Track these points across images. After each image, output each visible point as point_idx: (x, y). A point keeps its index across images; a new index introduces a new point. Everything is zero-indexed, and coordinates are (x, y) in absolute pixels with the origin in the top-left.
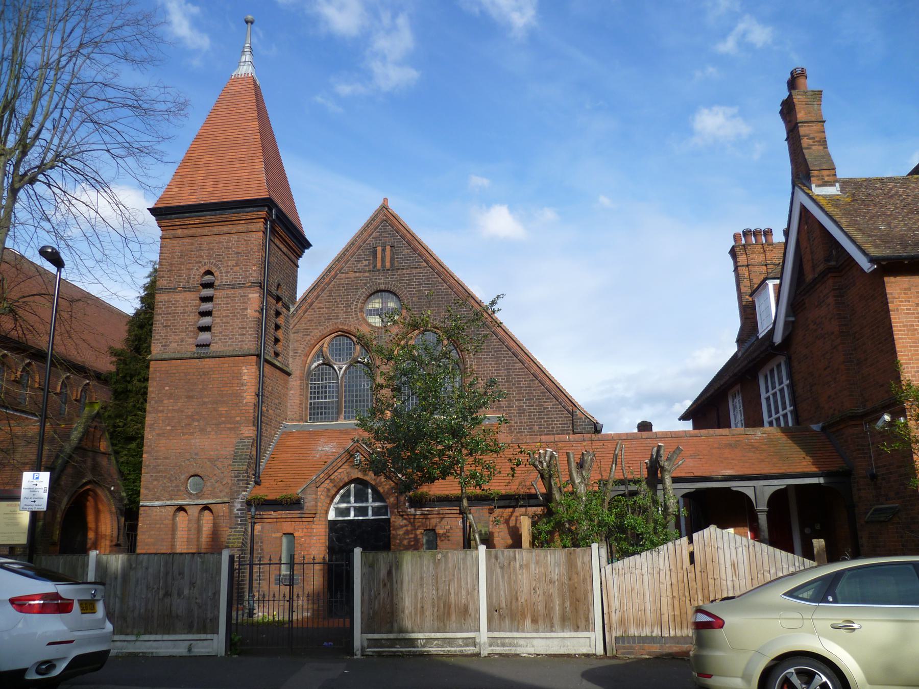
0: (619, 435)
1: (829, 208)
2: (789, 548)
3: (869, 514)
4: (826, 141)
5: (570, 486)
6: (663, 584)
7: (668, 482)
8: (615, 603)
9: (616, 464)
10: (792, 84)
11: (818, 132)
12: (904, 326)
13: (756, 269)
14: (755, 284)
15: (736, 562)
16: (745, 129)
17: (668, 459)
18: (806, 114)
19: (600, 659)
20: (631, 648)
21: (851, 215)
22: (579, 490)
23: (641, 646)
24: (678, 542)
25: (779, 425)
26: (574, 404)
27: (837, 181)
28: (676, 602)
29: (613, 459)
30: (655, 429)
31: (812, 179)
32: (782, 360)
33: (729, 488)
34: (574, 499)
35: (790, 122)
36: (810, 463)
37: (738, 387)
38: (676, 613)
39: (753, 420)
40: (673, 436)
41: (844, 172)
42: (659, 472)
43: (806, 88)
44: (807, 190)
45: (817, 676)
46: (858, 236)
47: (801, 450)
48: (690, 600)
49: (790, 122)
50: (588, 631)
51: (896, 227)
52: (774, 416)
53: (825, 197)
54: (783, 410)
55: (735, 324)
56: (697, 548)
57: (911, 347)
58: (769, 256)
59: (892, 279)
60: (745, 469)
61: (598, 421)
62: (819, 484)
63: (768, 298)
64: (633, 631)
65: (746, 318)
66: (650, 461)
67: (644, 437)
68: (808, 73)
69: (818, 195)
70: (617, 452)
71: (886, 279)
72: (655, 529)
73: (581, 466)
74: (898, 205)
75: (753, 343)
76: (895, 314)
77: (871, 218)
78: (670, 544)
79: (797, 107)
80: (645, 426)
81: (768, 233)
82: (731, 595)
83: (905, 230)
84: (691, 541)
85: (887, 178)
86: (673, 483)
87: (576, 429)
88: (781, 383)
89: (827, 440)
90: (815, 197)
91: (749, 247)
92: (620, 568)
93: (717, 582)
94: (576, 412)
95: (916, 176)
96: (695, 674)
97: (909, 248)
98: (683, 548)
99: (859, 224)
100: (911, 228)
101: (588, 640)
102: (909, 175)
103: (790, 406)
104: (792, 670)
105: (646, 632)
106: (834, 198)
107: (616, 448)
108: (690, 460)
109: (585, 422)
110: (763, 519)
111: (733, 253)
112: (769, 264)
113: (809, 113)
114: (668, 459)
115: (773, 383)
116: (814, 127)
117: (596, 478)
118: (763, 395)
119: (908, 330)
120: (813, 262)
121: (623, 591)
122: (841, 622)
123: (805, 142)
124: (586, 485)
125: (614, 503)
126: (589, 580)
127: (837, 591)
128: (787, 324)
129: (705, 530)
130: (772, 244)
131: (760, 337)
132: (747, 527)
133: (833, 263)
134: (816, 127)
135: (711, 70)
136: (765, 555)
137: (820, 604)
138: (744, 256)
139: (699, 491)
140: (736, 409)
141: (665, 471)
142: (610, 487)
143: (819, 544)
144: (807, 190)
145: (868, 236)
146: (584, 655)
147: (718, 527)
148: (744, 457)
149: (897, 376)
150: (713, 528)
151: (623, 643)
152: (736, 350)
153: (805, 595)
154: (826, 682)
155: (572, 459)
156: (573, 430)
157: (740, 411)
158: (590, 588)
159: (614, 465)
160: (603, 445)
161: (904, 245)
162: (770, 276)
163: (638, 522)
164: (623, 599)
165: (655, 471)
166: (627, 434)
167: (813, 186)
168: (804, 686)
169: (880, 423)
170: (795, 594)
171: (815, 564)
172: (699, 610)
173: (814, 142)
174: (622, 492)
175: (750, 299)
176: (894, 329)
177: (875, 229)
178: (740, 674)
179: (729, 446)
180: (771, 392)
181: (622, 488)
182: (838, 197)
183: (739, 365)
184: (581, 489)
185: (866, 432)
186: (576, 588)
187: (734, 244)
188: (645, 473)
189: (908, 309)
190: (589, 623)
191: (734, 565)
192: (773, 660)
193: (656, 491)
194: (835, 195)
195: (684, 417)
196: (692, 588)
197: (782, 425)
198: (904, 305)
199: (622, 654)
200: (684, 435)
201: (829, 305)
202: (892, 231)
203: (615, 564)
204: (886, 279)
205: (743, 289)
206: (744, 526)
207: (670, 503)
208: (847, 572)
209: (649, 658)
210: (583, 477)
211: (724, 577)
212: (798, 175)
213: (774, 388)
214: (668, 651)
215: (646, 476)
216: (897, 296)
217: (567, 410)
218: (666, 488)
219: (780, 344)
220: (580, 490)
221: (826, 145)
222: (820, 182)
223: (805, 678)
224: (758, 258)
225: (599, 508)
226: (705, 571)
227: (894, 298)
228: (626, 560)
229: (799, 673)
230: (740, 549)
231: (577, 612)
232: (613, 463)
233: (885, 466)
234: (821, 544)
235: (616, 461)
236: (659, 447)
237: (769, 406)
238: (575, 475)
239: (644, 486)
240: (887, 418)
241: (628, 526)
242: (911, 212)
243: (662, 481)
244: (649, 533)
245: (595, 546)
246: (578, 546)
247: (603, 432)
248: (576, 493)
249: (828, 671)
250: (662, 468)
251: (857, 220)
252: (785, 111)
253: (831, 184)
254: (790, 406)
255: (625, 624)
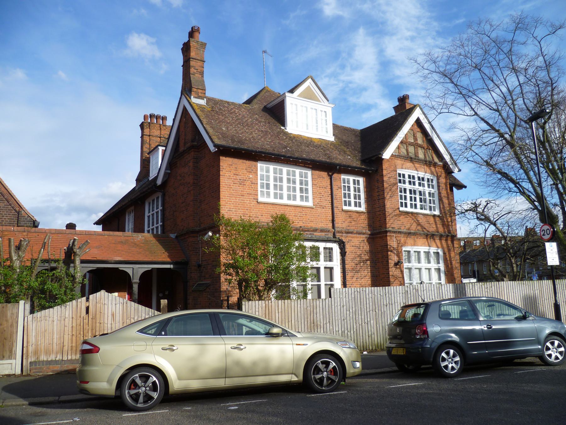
0: (50, 230)
1: (198, 112)
2: (150, 307)
3: (195, 286)
4: (203, 73)
5: (9, 261)
6: (66, 326)
7: (78, 262)
8: (32, 340)
9: (44, 249)
10: (191, 34)
11: (200, 67)
12: (226, 185)
13: (154, 138)
14: (152, 147)
15: (114, 313)
16: (158, 54)
17: (79, 248)
18: (196, 54)
19: (17, 377)
20: (40, 368)
21: (210, 118)
22: (15, 265)
23: (47, 367)
24: (79, 300)
25: (153, 233)
26: (20, 206)
27: (205, 97)
28: (74, 338)
29: (42, 245)
30: (77, 228)
31: (192, 93)
32: (160, 195)
33: (118, 268)
34: (10, 270)
35: (186, 56)
36: (167, 256)
37: (133, 208)
38: (73, 345)
39: (139, 229)
40: (87, 234)
41: (209, 93)
42: (72, 256)
43: (199, 40)
44: (188, 98)
45: (151, 378)
46: (211, 131)
47: (162, 248)
48: (83, 337)
49: (186, 56)
50: (11, 359)
51: (231, 130)
52: (151, 227)
53: (197, 105)
54: (156, 224)
55: (137, 169)
56: (91, 304)
57: (228, 196)
58: (163, 132)
59: (224, 158)
60: (129, 257)
61: (37, 220)
62: (170, 268)
63: (158, 157)
64: (43, 358)
65: (143, 167)
66: (68, 248)
67: (67, 233)
68: (201, 31)
69: (194, 103)
70: (45, 241)
71: (221, 157)
72: (65, 292)
73: (18, 248)
74: (234, 119)
75: (145, 183)
76: (223, 178)
77: (219, 122)
78: (74, 302)
79: (191, 49)
80: (71, 226)
81: (164, 119)
82: (106, 332)
83: (235, 133)
84: (88, 299)
85: (231, 102)
86: (81, 263)
87: (20, 223)
88: (157, 208)
89: (176, 242)
90: (192, 104)
91: (152, 125)
92: (38, 317)
93: (102, 325)
94: (21, 212)
95: (245, 105)
96: (78, 382)
97: (235, 143)
98: (83, 304)
99: (212, 124)
100: (238, 132)
101: (10, 365)
102: (243, 103)
103: (161, 222)
104: (137, 375)
105: (52, 357)
106: (203, 106)
107: (45, 238)
108: (96, 250)
109: (27, 219)
110: (135, 288)
111: (142, 126)
112: (162, 137)
113: (198, 54)
114: (79, 248)
115: (153, 208)
116: (199, 63)
117: (30, 257)
118: (147, 214)
119: (228, 187)
120: (185, 141)
121: (38, 331)
122: (167, 346)
123: (192, 70)
124: (21, 261)
125: (41, 274)
126: (15, 324)
127: (167, 329)
128: (165, 174)
129: (98, 293)
130: (165, 126)
131: (150, 179)
132: (126, 292)
133: (195, 143)
134: (199, 63)
135: (143, 11)
136: (133, 308)
137: (157, 337)
138: (149, 129)
139: (98, 269)
140: (129, 222)
141: (76, 255)
142: (38, 263)
143: (164, 302)
144: (188, 98)
145: (217, 132)
146: (6, 375)
147: (106, 292)
148: (130, 250)
149: (218, 212)
150: (103, 292)
151: (36, 365)
152: (135, 185)
153: (150, 332)
154: (155, 381)
155: (12, 243)
156: (18, 224)
157: (132, 222)
158: (15, 331)
159: (42, 250)
160: (38, 235)
161: (233, 141)
162: (161, 144)
163: (54, 287)
164: (38, 337)
165: (70, 254)
166: (56, 229)
167: (192, 97)
168: (143, 384)
169: (206, 237)
170: (144, 331)
171: (160, 313)
172: (85, 342)
173: (197, 72)
174: (47, 268)
175: (148, 156)
176: (221, 185)
177: (220, 129)
178: (106, 380)
179: (121, 242)
180: (151, 213)
181: (47, 264)
182: (204, 107)
183: (135, 195)
184: (17, 264)
185: (199, 241)
186: (5, 331)
187: (143, 121)
188: (63, 256)
189: (229, 176)
190: (12, 354)
191: (113, 315)
192: (127, 370)
193: (69, 268)
194: (203, 105)
195: (97, 223)
196: (85, 328)
197: (155, 233)
198: (228, 174)
199: (34, 373)
200: (94, 234)
201: (190, 166)
202: (228, 132)
203: (35, 315)
204: (221, 157)
205: (145, 149)
206: (124, 292)
207: (77, 275)
208: (174, 318)
209: (52, 374)
210: (19, 256)
211: (106, 322)
212: (185, 88)
213: (153, 210)
214: (66, 369)
215: (64, 258)
216: (225, 168)
217: (15, 210)
218: (76, 266)
219: (160, 185)
220: (16, 265)
221: (203, 75)
222: (196, 96)
223: (144, 379)
224: (156, 132)
225: (28, 277)
226: (95, 318)
227: (223, 169)
228: (43, 312)
229: (141, 376)
230: (118, 305)
231: (4, 347)
232: (42, 248)
233: (206, 260)
234: (165, 302)
235: (44, 247)
236: (75, 239)
237: (149, 221)
238: (13, 254)
239: (61, 264)
240: (210, 234)
241: (47, 289)
242: (239, 123)
243: (73, 262)
244: (61, 294)
245: (22, 303)
246: (10, 302)
247: (39, 227)
248: (12, 266)
249: (157, 374)
250: (75, 253)
251: (212, 122)
252: (184, 49)
253: (202, 98)
254: (161, 222)
255: (38, 353)
